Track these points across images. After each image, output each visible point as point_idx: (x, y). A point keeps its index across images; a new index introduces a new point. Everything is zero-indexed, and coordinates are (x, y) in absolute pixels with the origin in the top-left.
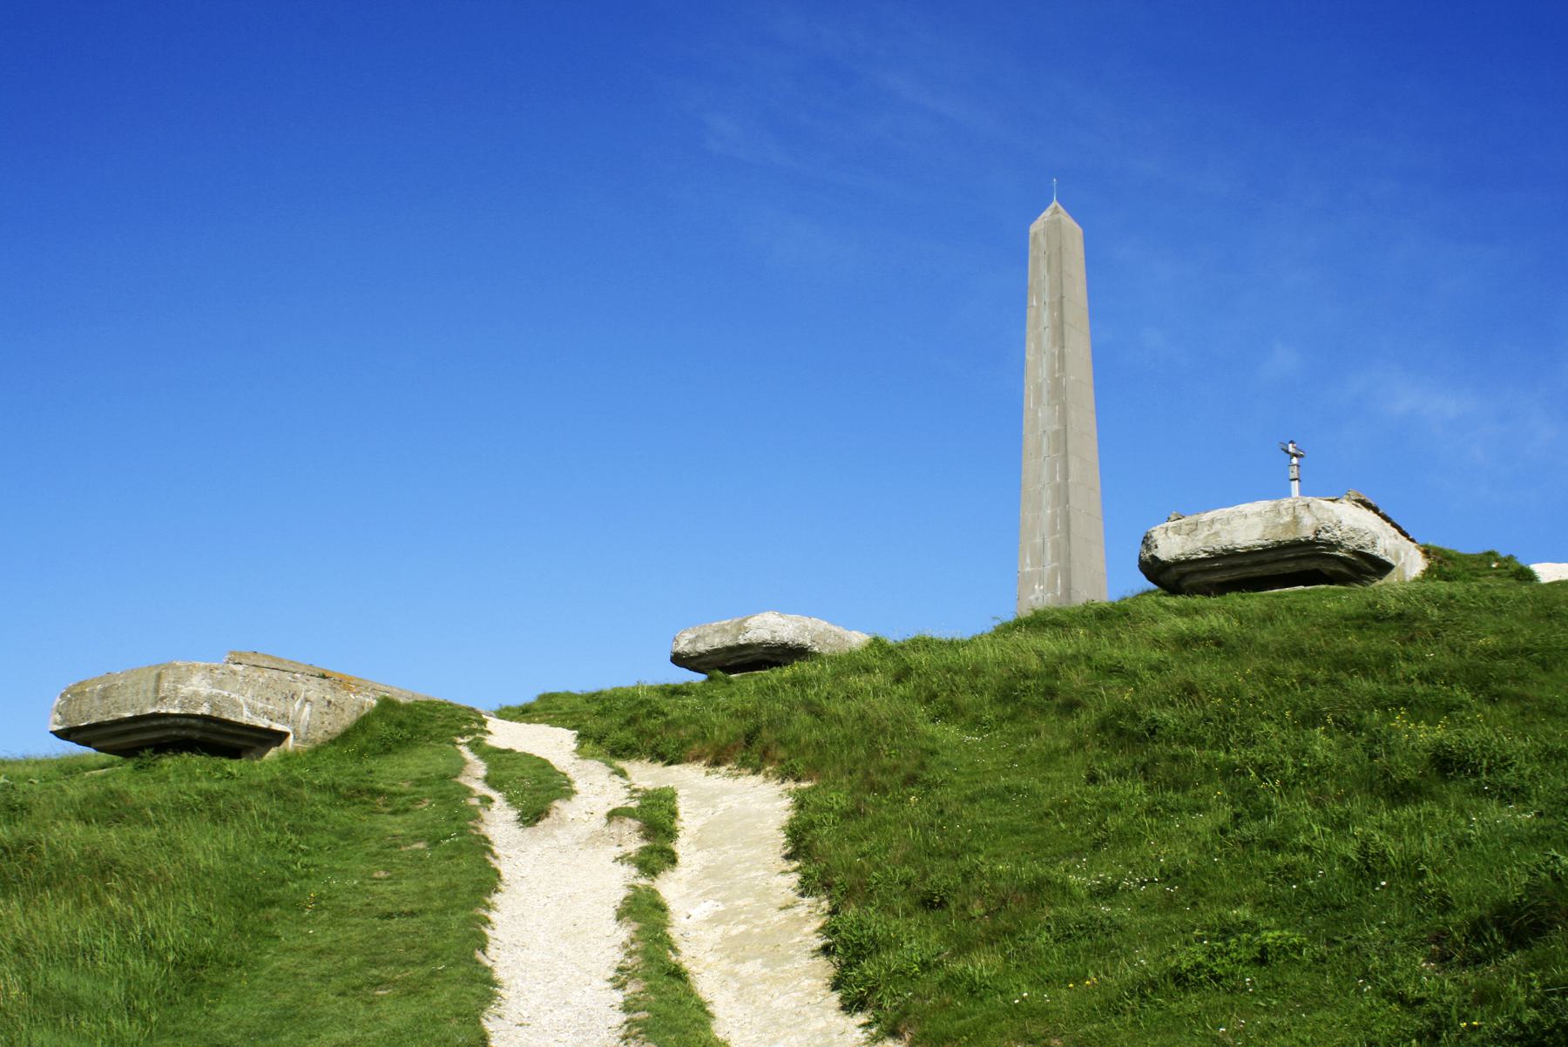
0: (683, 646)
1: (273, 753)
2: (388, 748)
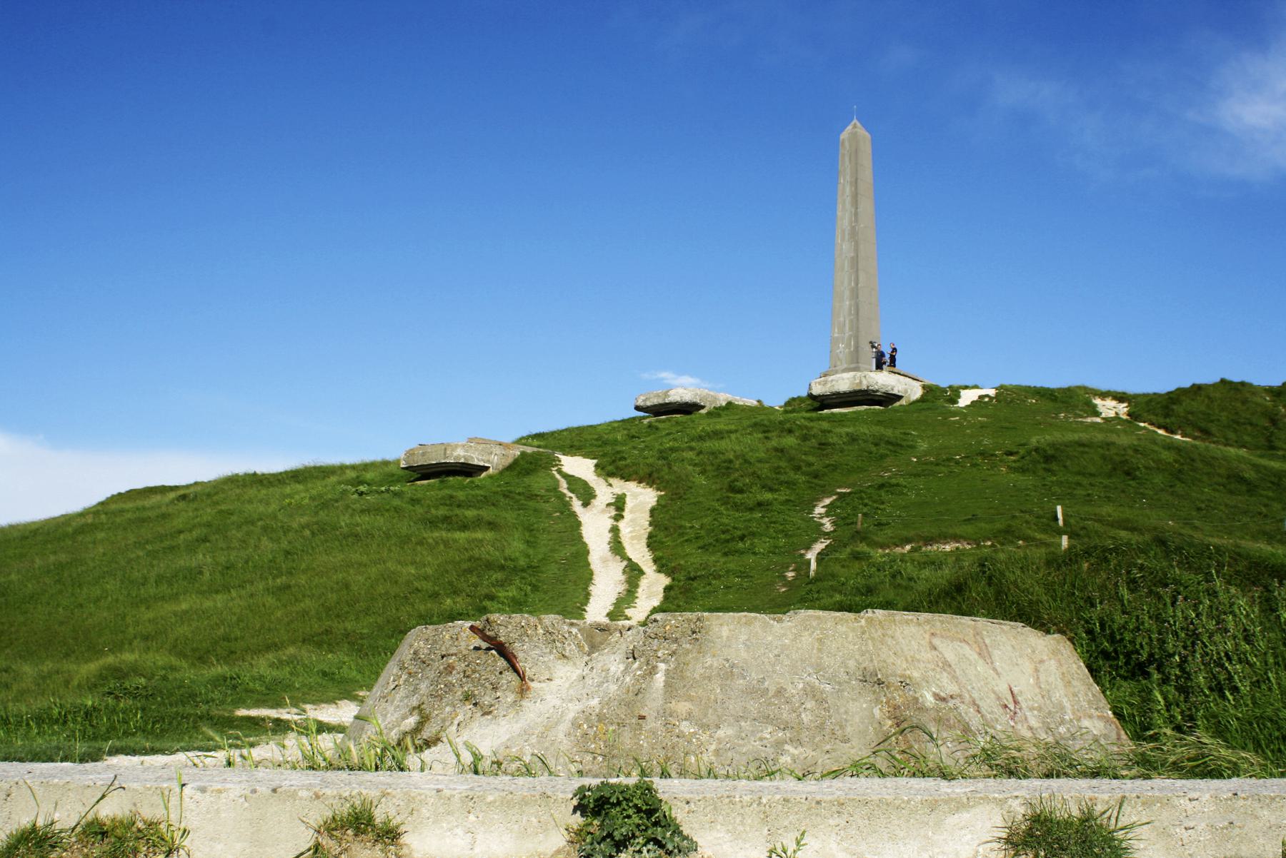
0: (640, 403)
1: (484, 475)
2: (528, 472)
